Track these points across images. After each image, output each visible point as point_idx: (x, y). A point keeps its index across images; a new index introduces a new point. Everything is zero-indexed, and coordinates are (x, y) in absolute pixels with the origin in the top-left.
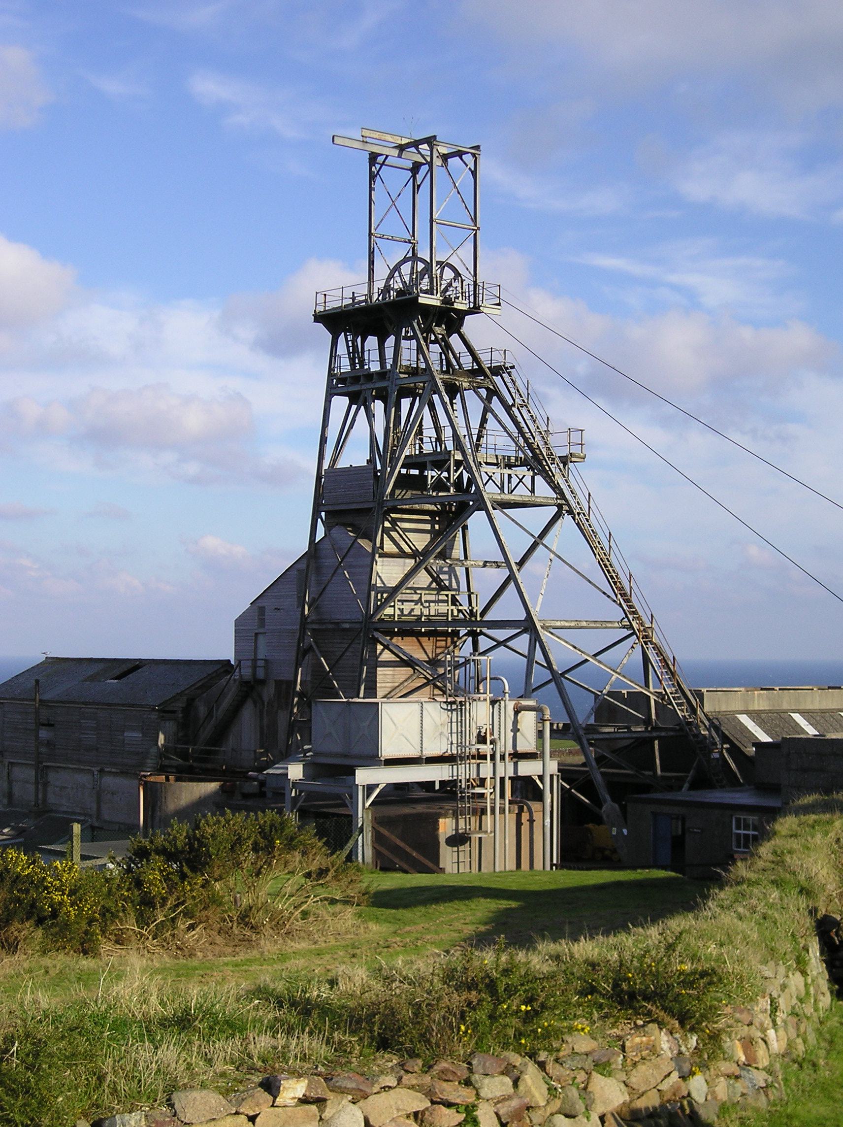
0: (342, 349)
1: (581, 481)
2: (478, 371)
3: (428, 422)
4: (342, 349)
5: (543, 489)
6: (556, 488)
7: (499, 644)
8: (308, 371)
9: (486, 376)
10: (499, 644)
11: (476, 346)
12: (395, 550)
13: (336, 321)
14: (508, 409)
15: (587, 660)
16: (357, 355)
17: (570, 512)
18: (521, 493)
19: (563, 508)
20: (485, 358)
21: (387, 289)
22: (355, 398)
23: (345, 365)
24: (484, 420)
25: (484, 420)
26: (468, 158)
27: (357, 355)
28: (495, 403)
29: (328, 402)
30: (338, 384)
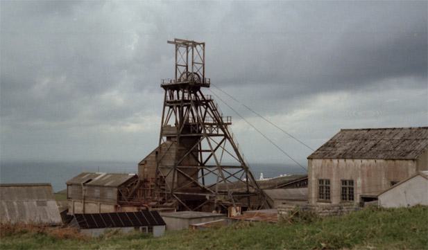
0: (168, 94)
1: (232, 129)
2: (205, 100)
3: (190, 114)
4: (168, 94)
5: (221, 132)
6: (224, 131)
7: (231, 175)
8: (160, 96)
9: (206, 102)
10: (231, 175)
11: (203, 94)
12: (223, 133)
13: (165, 87)
14: (212, 111)
15: (192, 176)
16: (172, 96)
17: (228, 138)
18: (215, 132)
19: (226, 136)
20: (206, 97)
21: (180, 80)
22: (171, 107)
23: (169, 99)
24: (205, 114)
25: (205, 114)
26: (202, 45)
27: (172, 96)
28: (208, 109)
29: (164, 108)
30: (166, 103)
